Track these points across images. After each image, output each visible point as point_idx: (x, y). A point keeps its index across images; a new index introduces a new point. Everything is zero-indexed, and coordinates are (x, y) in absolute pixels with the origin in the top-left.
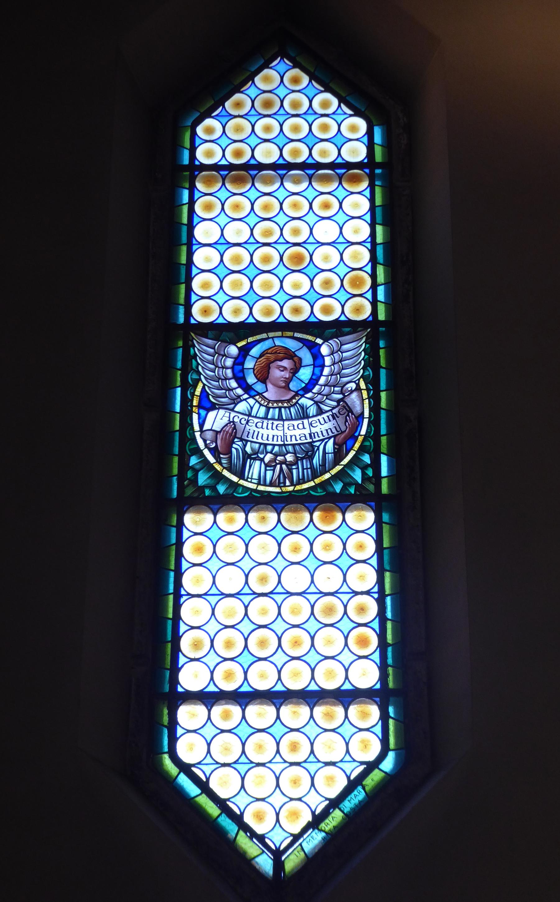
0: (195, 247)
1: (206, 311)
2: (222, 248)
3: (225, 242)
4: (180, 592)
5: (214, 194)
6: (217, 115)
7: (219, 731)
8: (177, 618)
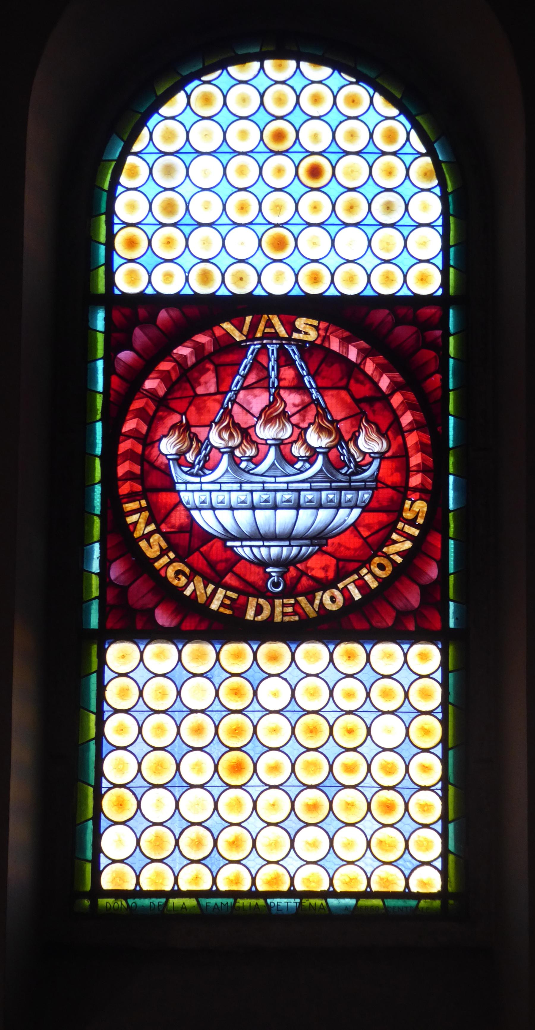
4: (113, 291)
5: (393, 261)
7: (129, 748)
8: (98, 850)
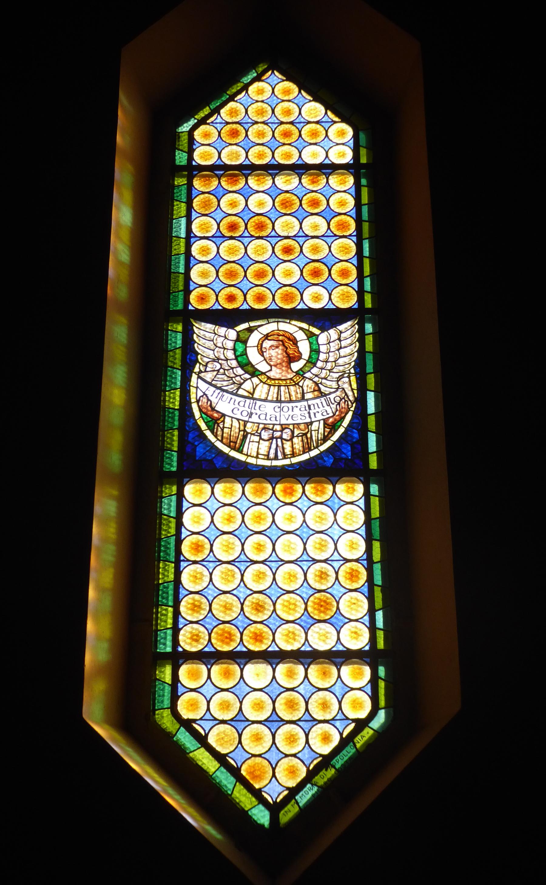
0: (193, 240)
1: (202, 298)
2: (218, 241)
3: (221, 235)
4: (180, 557)
6: (212, 122)
